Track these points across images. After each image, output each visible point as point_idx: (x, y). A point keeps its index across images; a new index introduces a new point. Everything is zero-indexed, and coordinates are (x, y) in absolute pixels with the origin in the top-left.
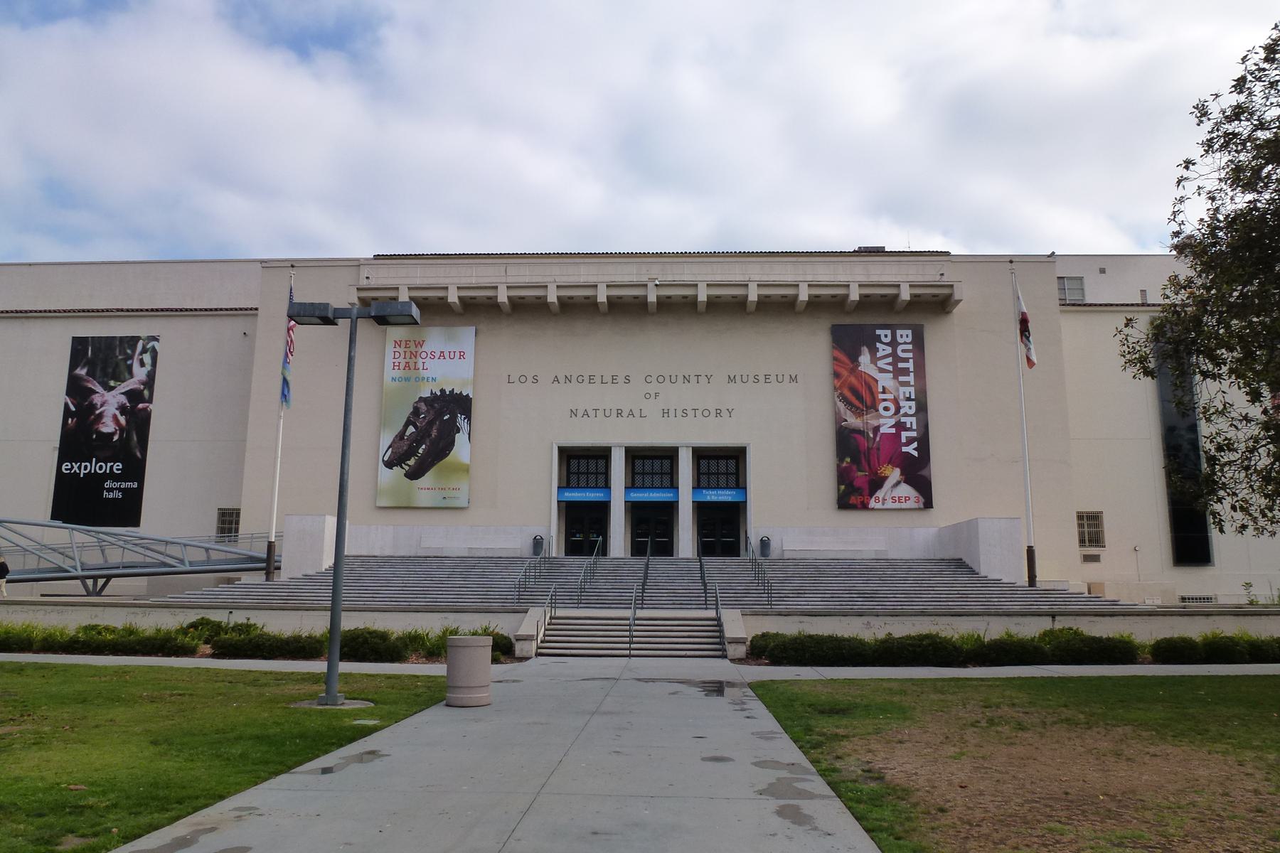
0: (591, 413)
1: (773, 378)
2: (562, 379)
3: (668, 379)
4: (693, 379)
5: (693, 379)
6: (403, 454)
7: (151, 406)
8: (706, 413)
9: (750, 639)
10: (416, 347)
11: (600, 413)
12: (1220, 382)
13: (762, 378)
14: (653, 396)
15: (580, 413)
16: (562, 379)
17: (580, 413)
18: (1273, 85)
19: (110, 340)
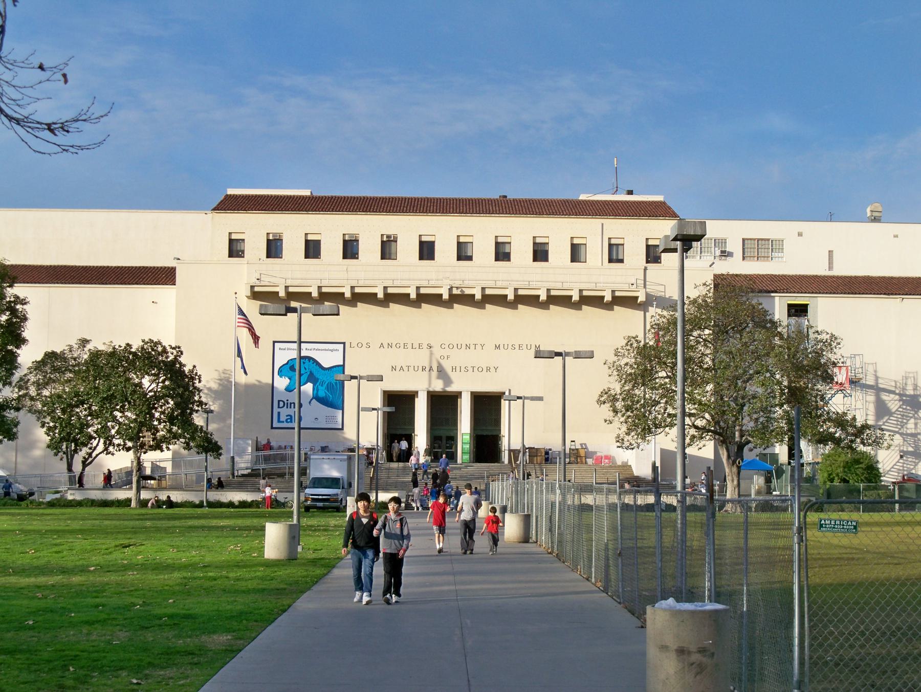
0: (406, 369)
1: (524, 347)
2: (386, 345)
3: (455, 346)
4: (472, 347)
5: (472, 347)
6: (834, 443)
7: (18, 351)
8: (480, 370)
9: (18, 351)
10: (715, 259)
11: (411, 369)
12: (539, 346)
13: (517, 347)
14: (446, 357)
15: (398, 369)
16: (386, 345)
17: (398, 369)
18: (890, 689)
19: (314, 487)
